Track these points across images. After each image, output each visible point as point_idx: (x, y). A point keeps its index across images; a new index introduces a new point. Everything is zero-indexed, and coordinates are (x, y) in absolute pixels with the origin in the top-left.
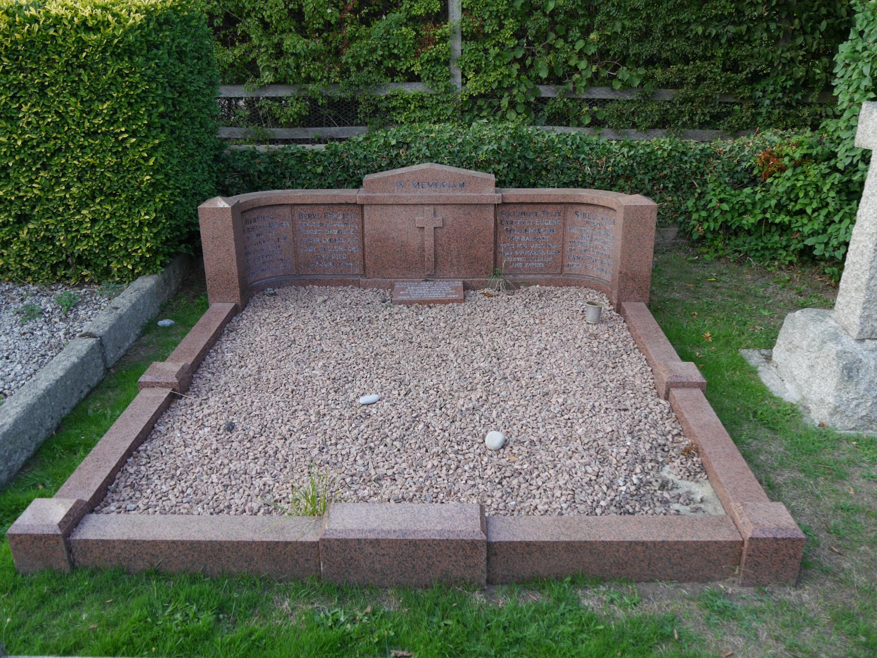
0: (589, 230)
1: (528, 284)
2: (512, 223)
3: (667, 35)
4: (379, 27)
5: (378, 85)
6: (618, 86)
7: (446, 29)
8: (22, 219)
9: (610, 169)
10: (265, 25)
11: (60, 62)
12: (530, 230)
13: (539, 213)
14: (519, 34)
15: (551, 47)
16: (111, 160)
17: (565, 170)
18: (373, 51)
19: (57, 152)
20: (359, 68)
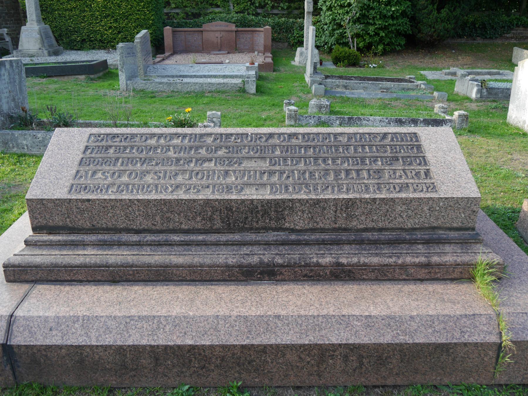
5: (207, 9)
6: (280, 8)
8: (119, 32)
16: (143, 17)
19: (130, 15)
20: (201, 3)
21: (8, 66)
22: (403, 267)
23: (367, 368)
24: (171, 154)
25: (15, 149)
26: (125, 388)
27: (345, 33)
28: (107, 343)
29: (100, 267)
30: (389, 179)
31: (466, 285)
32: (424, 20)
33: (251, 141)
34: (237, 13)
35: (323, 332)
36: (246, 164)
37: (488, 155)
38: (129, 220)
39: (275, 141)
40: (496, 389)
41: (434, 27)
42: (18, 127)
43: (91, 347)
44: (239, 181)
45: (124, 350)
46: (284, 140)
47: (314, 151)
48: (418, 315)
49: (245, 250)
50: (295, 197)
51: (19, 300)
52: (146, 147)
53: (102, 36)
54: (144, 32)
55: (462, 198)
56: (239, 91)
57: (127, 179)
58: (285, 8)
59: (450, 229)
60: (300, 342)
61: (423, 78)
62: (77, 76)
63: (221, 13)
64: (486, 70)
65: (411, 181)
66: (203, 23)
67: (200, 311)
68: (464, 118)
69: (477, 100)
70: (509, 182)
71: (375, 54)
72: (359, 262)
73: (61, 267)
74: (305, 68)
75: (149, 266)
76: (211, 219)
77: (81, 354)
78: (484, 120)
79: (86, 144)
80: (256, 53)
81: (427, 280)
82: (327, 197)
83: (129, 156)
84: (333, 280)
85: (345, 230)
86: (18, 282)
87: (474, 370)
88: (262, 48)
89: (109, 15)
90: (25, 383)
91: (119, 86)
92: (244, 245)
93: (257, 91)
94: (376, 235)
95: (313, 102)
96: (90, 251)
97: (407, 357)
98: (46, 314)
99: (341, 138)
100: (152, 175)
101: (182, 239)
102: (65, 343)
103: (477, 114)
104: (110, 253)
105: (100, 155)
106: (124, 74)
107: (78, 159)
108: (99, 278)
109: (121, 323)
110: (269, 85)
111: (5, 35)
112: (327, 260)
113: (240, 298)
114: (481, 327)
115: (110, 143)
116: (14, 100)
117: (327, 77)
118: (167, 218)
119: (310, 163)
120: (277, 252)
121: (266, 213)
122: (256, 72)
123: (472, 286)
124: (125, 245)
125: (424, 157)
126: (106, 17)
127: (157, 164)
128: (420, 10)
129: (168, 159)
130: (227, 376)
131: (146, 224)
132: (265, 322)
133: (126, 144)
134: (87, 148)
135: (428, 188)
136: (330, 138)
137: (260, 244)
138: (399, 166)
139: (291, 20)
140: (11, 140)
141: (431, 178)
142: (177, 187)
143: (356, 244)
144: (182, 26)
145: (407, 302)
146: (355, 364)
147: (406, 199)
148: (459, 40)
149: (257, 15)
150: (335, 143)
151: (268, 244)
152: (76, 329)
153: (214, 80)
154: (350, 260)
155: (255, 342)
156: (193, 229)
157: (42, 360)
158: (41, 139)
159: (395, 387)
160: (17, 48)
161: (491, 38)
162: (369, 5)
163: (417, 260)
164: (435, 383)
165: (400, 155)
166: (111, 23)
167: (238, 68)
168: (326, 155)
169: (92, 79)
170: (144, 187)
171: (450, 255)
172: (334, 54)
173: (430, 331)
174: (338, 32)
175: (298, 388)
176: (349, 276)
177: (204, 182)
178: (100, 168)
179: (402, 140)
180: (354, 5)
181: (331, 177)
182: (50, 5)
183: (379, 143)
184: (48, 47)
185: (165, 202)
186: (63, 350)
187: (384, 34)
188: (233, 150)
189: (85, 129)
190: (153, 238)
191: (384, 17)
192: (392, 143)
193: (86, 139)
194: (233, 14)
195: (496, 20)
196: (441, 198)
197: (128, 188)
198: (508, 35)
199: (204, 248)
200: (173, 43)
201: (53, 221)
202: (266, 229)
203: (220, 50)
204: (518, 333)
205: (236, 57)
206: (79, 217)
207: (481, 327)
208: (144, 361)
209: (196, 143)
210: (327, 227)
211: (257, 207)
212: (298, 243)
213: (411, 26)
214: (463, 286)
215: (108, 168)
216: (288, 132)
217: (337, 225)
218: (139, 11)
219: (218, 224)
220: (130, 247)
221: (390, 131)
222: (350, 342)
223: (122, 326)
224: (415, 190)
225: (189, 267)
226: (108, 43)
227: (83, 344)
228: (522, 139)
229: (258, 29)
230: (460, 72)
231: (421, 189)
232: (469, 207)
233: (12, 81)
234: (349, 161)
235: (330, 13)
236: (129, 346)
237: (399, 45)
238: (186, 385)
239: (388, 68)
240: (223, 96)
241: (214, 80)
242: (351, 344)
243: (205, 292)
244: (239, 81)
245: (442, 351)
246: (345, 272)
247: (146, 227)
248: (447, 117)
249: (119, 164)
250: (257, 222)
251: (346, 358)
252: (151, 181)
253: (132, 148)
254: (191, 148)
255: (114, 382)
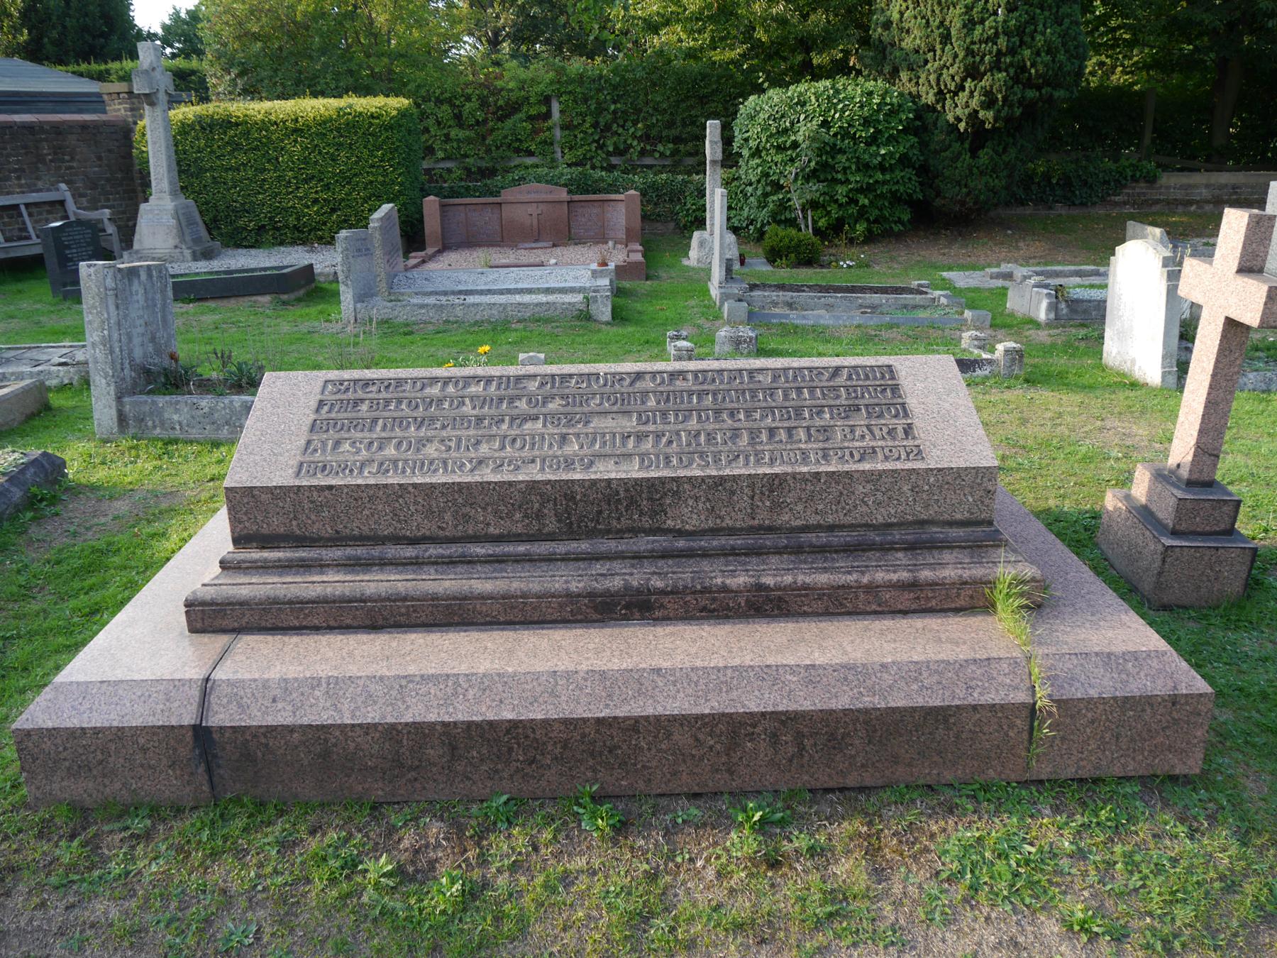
3: (684, 125)
4: (509, 123)
5: (510, 159)
6: (657, 155)
7: (550, 122)
8: (333, 210)
10: (439, 123)
11: (360, 132)
14: (595, 125)
15: (616, 133)
16: (380, 178)
18: (506, 137)
19: (355, 175)
20: (498, 148)
21: (143, 276)
22: (872, 588)
23: (811, 756)
24: (467, 409)
25: (158, 430)
26: (398, 803)
27: (789, 200)
28: (369, 721)
29: (350, 601)
30: (842, 441)
31: (980, 618)
32: (947, 173)
33: (605, 385)
34: (569, 165)
35: (734, 694)
36: (596, 423)
37: (1058, 421)
38: (399, 521)
39: (648, 384)
40: (1034, 789)
41: (966, 186)
42: (163, 390)
43: (342, 727)
44: (586, 450)
45: (399, 732)
46: (663, 382)
47: (715, 399)
48: (894, 663)
49: (599, 568)
50: (682, 473)
51: (216, 658)
52: (423, 399)
53: (298, 219)
54: (386, 207)
55: (966, 469)
56: (578, 318)
57: (393, 452)
58: (668, 153)
59: (951, 524)
60: (696, 711)
61: (947, 285)
62: (254, 298)
63: (537, 166)
64: (1072, 268)
65: (880, 443)
66: (502, 188)
67: (524, 666)
68: (1015, 356)
69: (1049, 325)
70: (1092, 466)
71: (851, 241)
72: (795, 583)
73: (284, 603)
74: (708, 271)
75: (435, 597)
76: (539, 516)
77: (326, 740)
78: (1060, 362)
79: (319, 397)
80: (611, 243)
81: (914, 612)
82: (736, 472)
83: (395, 414)
84: (752, 616)
85: (770, 529)
86: (209, 632)
87: (993, 755)
88: (622, 235)
89: (313, 177)
90: (229, 796)
91: (340, 313)
92: (597, 559)
93: (613, 318)
94: (823, 538)
95: (723, 332)
96: (331, 576)
97: (879, 733)
98: (266, 676)
99: (761, 378)
100: (436, 444)
101: (490, 552)
102: (299, 722)
103: (1048, 350)
104: (367, 578)
105: (345, 415)
106: (350, 291)
107: (309, 421)
108: (349, 622)
109: (392, 688)
110: (638, 306)
111: (106, 221)
112: (741, 580)
113: (591, 646)
114: (1001, 678)
115: (360, 394)
116: (153, 339)
117: (753, 287)
118: (464, 516)
119: (708, 418)
120: (653, 569)
121: (632, 502)
122: (611, 281)
123: (990, 619)
124: (392, 564)
125: (903, 405)
126: (306, 181)
127: (444, 427)
128: (936, 152)
129: (463, 418)
130: (573, 777)
131: (428, 527)
132: (635, 679)
133: (389, 396)
134: (321, 403)
135: (908, 455)
136: (742, 377)
137: (624, 558)
138: (860, 420)
139: (680, 177)
140: (151, 413)
141: (914, 438)
142: (480, 462)
143: (790, 553)
144: (459, 195)
145: (877, 644)
146: (792, 750)
147: (872, 472)
148: (1020, 210)
149: (611, 168)
150: (751, 386)
151: (637, 557)
152: (317, 699)
153: (527, 298)
154: (779, 579)
155: (620, 713)
156: (509, 535)
157: (259, 754)
158: (206, 410)
159: (862, 789)
160: (132, 246)
161: (1083, 204)
162: (835, 145)
163: (894, 577)
164: (929, 780)
165: (861, 402)
166: (316, 192)
167: (575, 274)
168: (736, 405)
169: (284, 303)
170: (423, 464)
171: (950, 568)
172: (767, 241)
173: (915, 687)
174: (775, 198)
175: (696, 796)
176: (779, 608)
177: (526, 453)
178: (346, 436)
179: (867, 377)
180: (804, 146)
181: (744, 440)
182: (196, 159)
183: (826, 384)
184: (190, 244)
185: (460, 487)
186: (295, 735)
187: (866, 202)
188: (574, 401)
189: (315, 373)
190: (440, 551)
191: (865, 167)
192: (849, 383)
193: (318, 389)
194: (562, 168)
195: (1091, 169)
196: (931, 470)
197: (396, 467)
198: (1117, 198)
199: (527, 565)
200: (443, 228)
201: (266, 524)
202: (635, 531)
203: (536, 241)
204: (1062, 687)
205: (571, 252)
206: (313, 517)
207: (1001, 678)
208: (432, 752)
209: (510, 392)
210: (738, 524)
211: (618, 493)
212: (689, 554)
213: (921, 184)
214: (974, 619)
215: (359, 435)
216: (669, 369)
217: (756, 522)
218: (372, 166)
219: (551, 525)
220: (400, 568)
221: (846, 364)
222: (780, 708)
223: (394, 693)
224: (886, 458)
225: (504, 598)
226: (310, 231)
227: (329, 722)
228: (1128, 393)
229: (613, 196)
230: (1020, 271)
231: (897, 455)
232: (980, 484)
233: (150, 304)
234: (774, 413)
235: (758, 161)
236: (407, 724)
237: (900, 221)
238: (503, 794)
239: (877, 268)
240: (547, 329)
241: (527, 298)
242: (781, 713)
243: (532, 639)
244: (578, 298)
245: (937, 721)
246: (771, 601)
247: (428, 533)
248: (985, 356)
249: (378, 429)
250: (619, 519)
251: (774, 737)
252: (435, 455)
253: (400, 401)
254: (501, 400)
255: (380, 793)
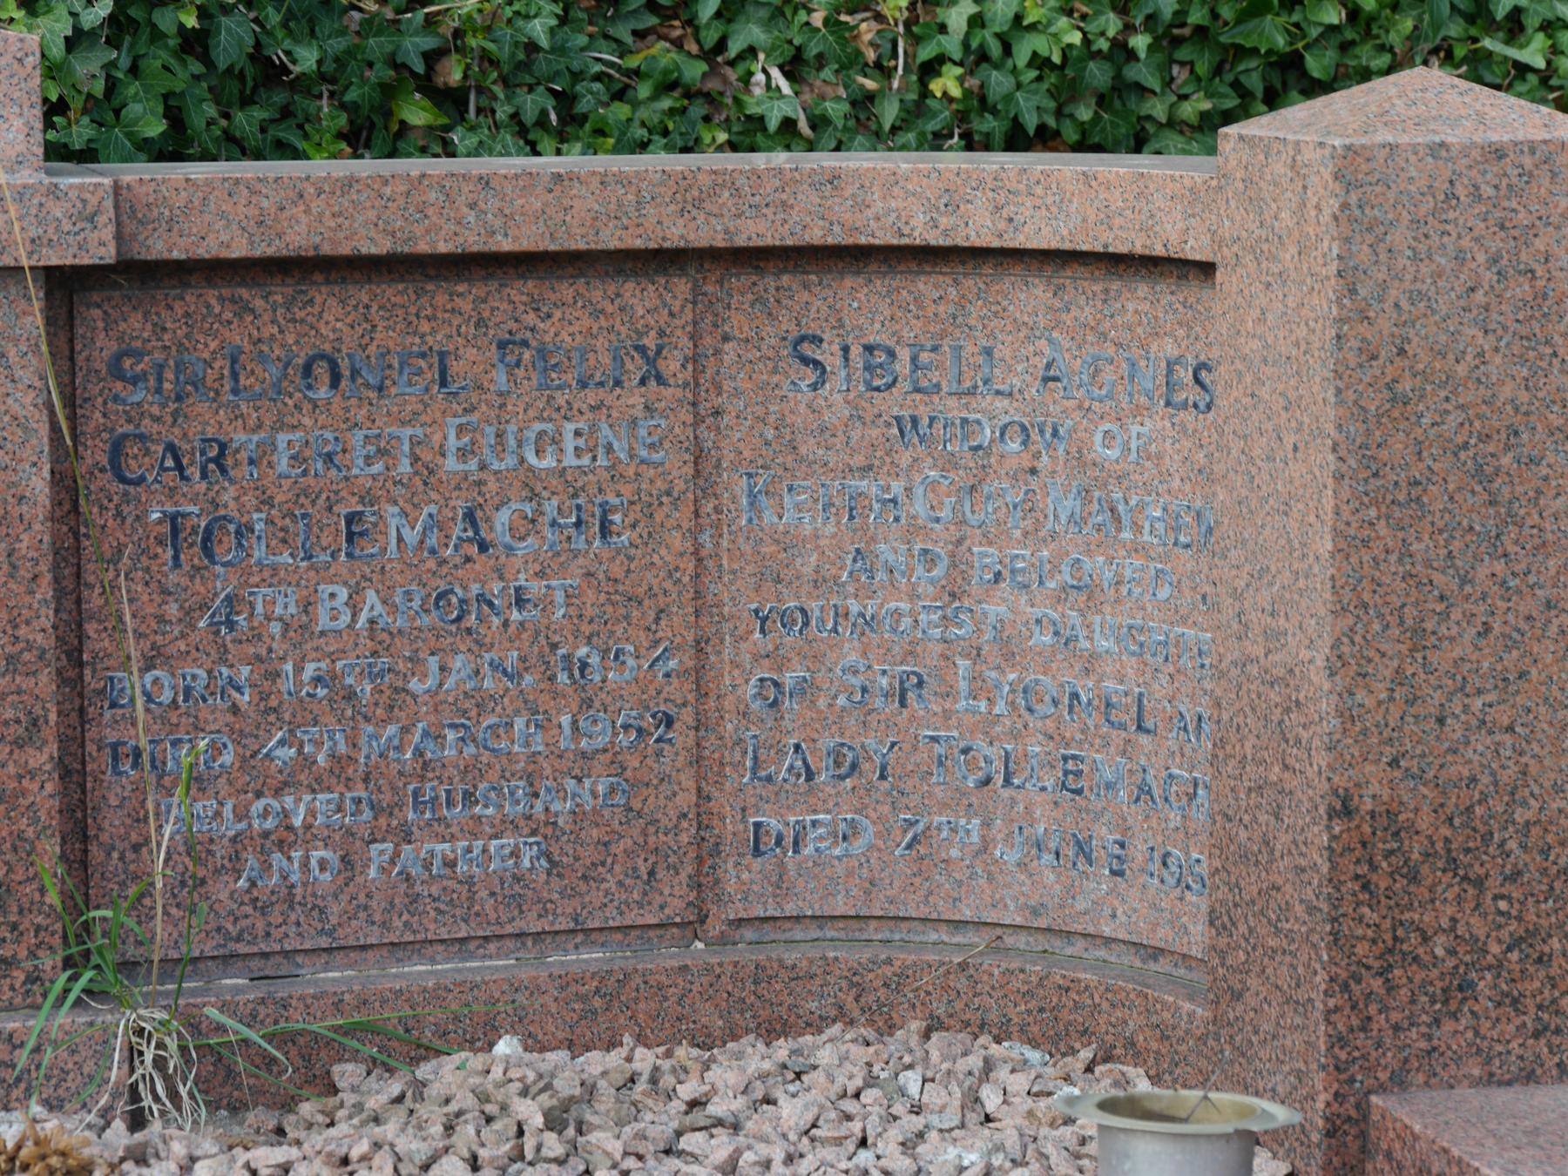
0: (924, 489)
1: (404, 1044)
2: (220, 458)
9: (948, 83)
12: (398, 528)
13: (469, 361)
17: (589, 98)
